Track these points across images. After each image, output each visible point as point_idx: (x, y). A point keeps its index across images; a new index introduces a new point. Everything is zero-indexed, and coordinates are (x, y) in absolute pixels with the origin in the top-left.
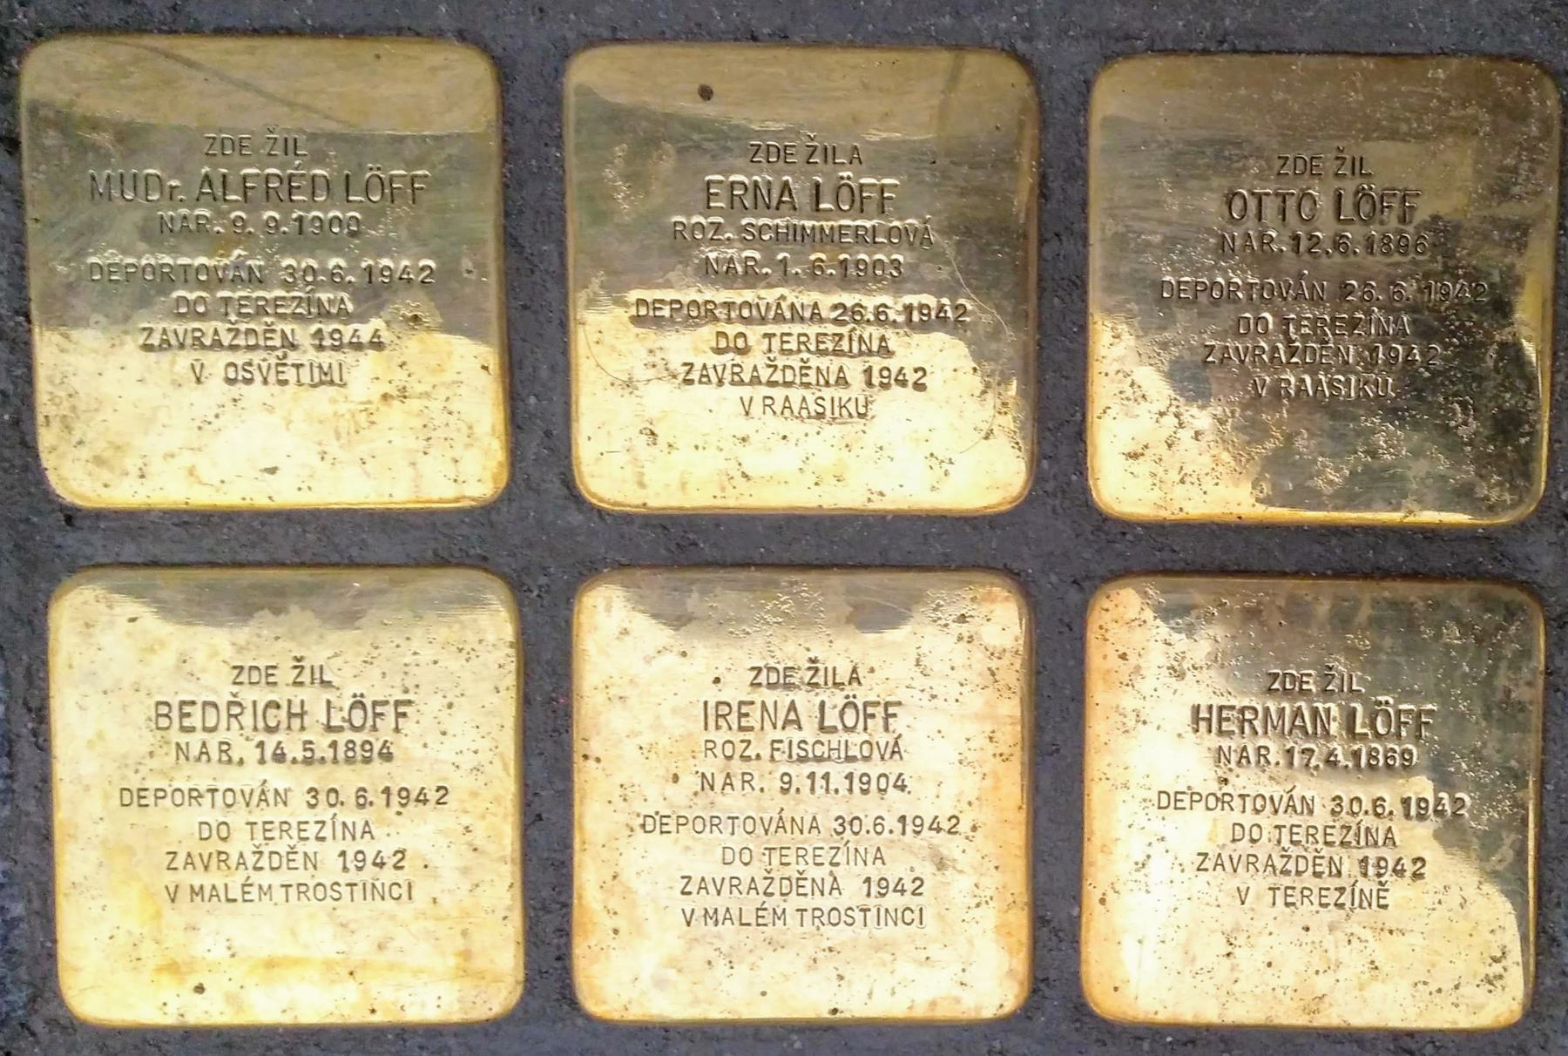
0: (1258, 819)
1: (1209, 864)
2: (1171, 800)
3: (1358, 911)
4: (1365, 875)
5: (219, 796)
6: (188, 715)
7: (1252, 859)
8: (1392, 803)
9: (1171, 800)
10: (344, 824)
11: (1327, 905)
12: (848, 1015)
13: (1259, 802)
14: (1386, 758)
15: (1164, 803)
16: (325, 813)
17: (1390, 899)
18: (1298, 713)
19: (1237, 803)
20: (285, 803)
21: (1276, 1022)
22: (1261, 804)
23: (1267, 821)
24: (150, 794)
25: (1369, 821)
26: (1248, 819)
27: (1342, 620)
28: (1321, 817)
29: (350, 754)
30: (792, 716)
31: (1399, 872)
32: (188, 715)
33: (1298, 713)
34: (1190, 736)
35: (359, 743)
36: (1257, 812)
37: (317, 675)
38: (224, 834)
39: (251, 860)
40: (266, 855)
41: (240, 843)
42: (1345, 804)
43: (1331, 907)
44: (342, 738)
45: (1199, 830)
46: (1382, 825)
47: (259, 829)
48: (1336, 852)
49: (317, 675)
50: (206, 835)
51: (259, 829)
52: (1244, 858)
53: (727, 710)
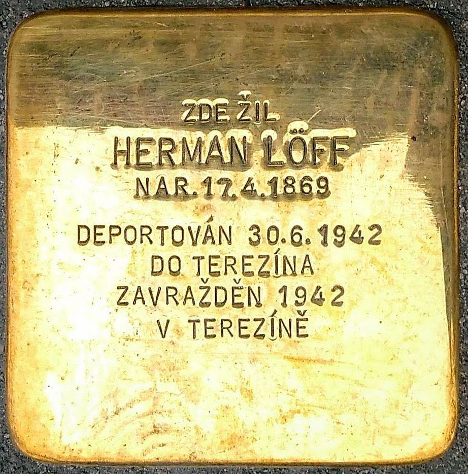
0: (177, 251)
1: (129, 298)
2: (91, 235)
3: (278, 340)
4: (284, 304)
5: (167, 233)
6: (146, 152)
7: (172, 292)
8: (310, 232)
9: (91, 235)
10: (285, 258)
11: (248, 336)
12: (162, 460)
13: (178, 233)
14: (302, 186)
15: (84, 237)
16: (264, 248)
17: (309, 327)
18: (215, 144)
19: (156, 235)
20: (230, 242)
21: (200, 457)
22: (177, 235)
23: (186, 251)
24: (105, 232)
25: (288, 250)
26: (167, 252)
27: (256, 53)
28: (240, 247)
29: (289, 190)
30: (215, 153)
31: (318, 301)
32: (146, 152)
33: (215, 144)
34: (108, 170)
35: (315, 179)
36: (175, 243)
37: (261, 114)
38: (175, 268)
39: (198, 295)
40: (212, 290)
41: (190, 277)
42: (263, 233)
43: (252, 338)
44: (281, 175)
45: (121, 263)
46: (299, 253)
47: (204, 264)
48: (255, 282)
49: (261, 114)
50: (157, 268)
51: (204, 264)
52: (163, 291)
53: (169, 147)
